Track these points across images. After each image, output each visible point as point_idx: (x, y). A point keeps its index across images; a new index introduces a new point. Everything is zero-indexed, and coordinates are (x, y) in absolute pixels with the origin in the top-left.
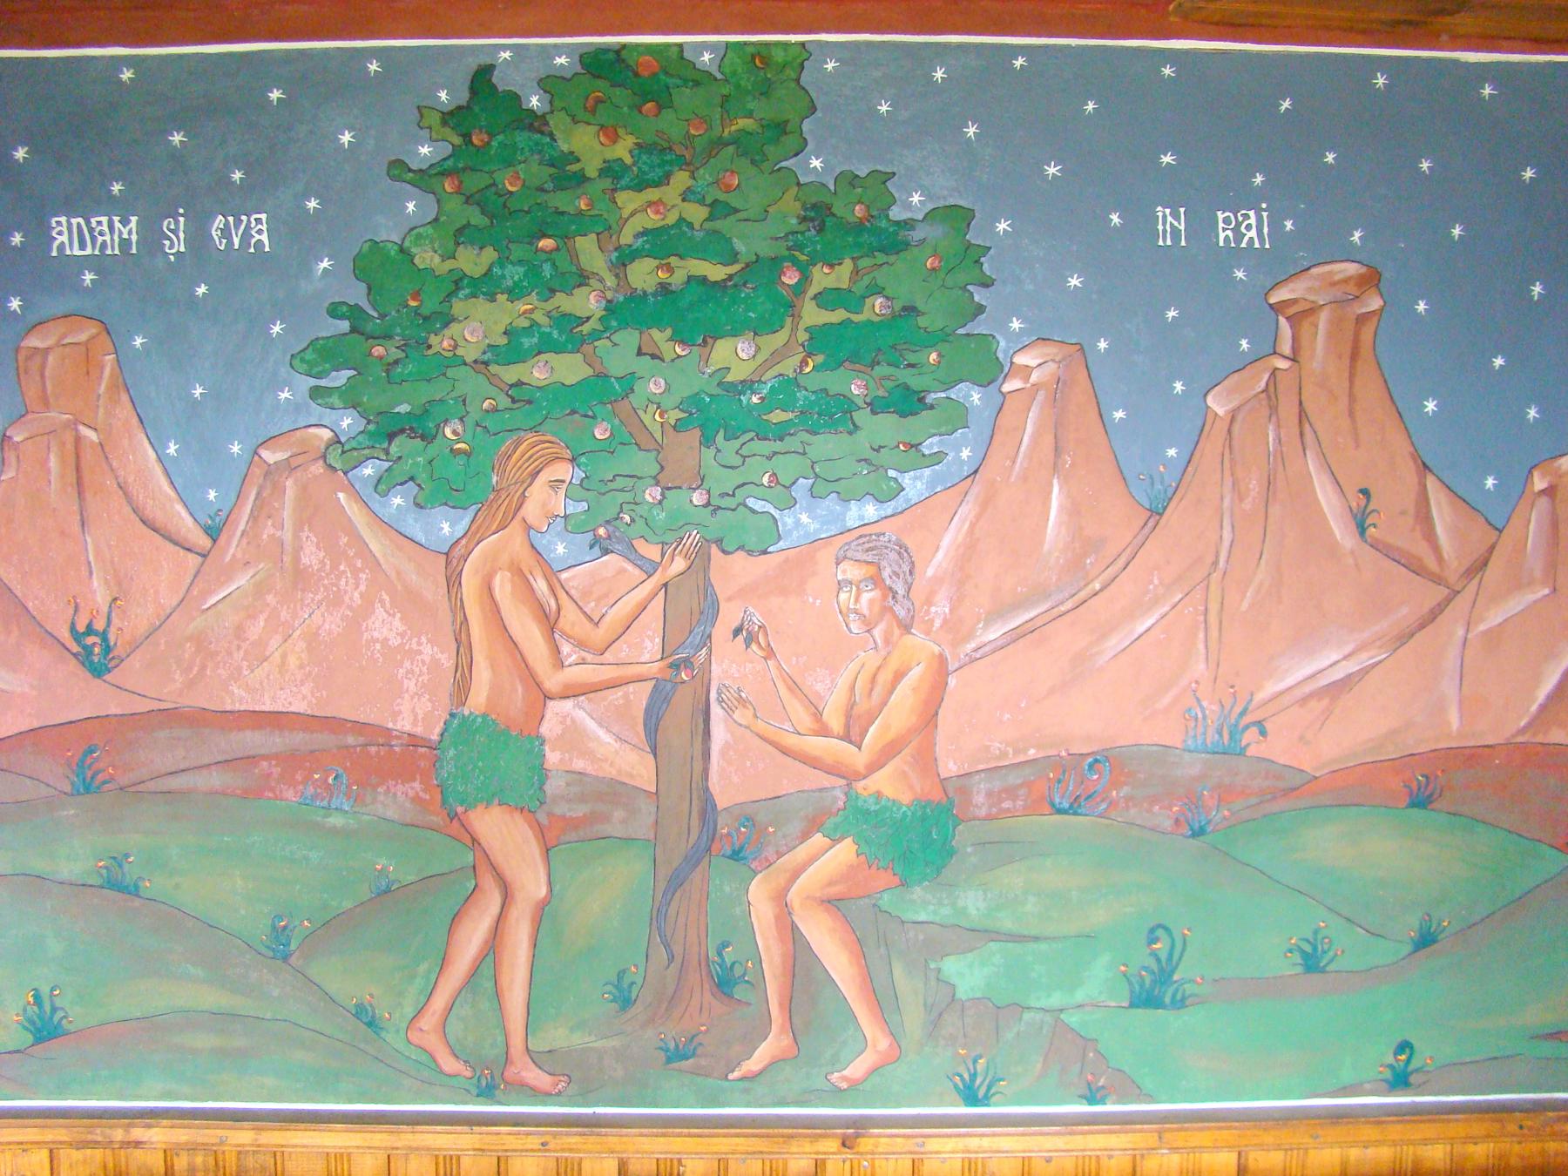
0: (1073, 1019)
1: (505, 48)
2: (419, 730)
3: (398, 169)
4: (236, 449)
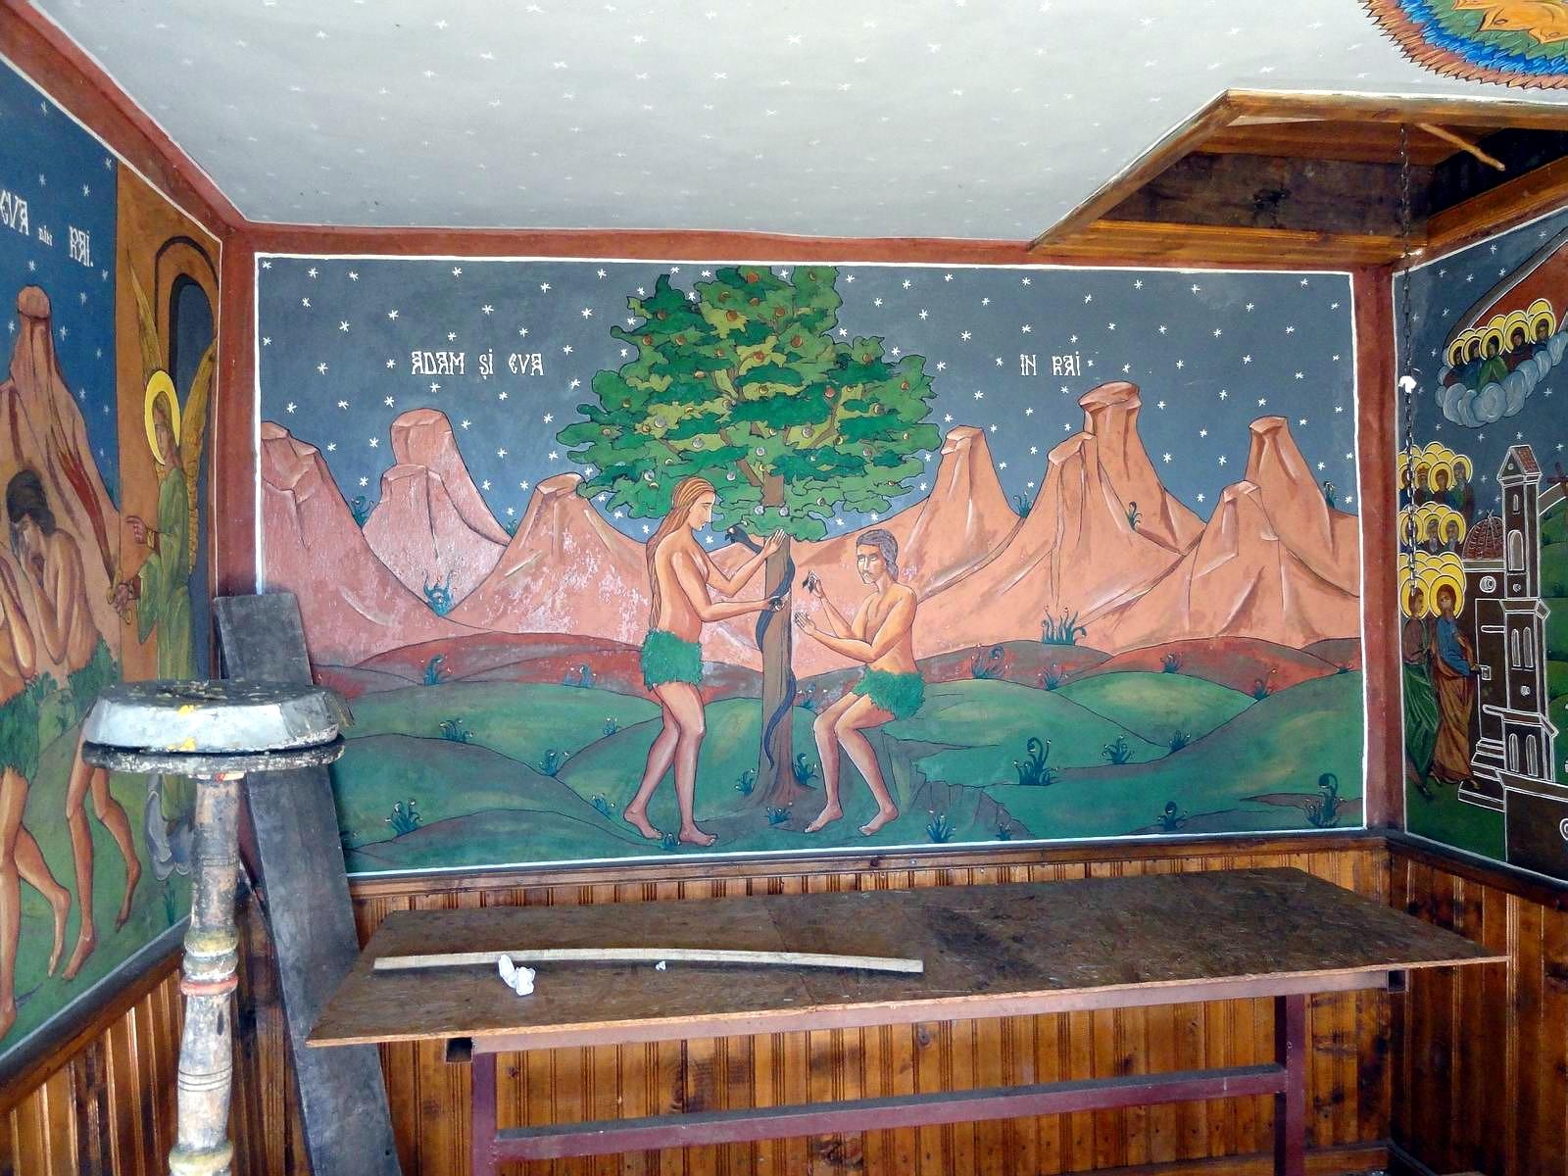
0: (990, 792)
1: (675, 265)
2: (631, 642)
3: (616, 331)
4: (524, 486)
